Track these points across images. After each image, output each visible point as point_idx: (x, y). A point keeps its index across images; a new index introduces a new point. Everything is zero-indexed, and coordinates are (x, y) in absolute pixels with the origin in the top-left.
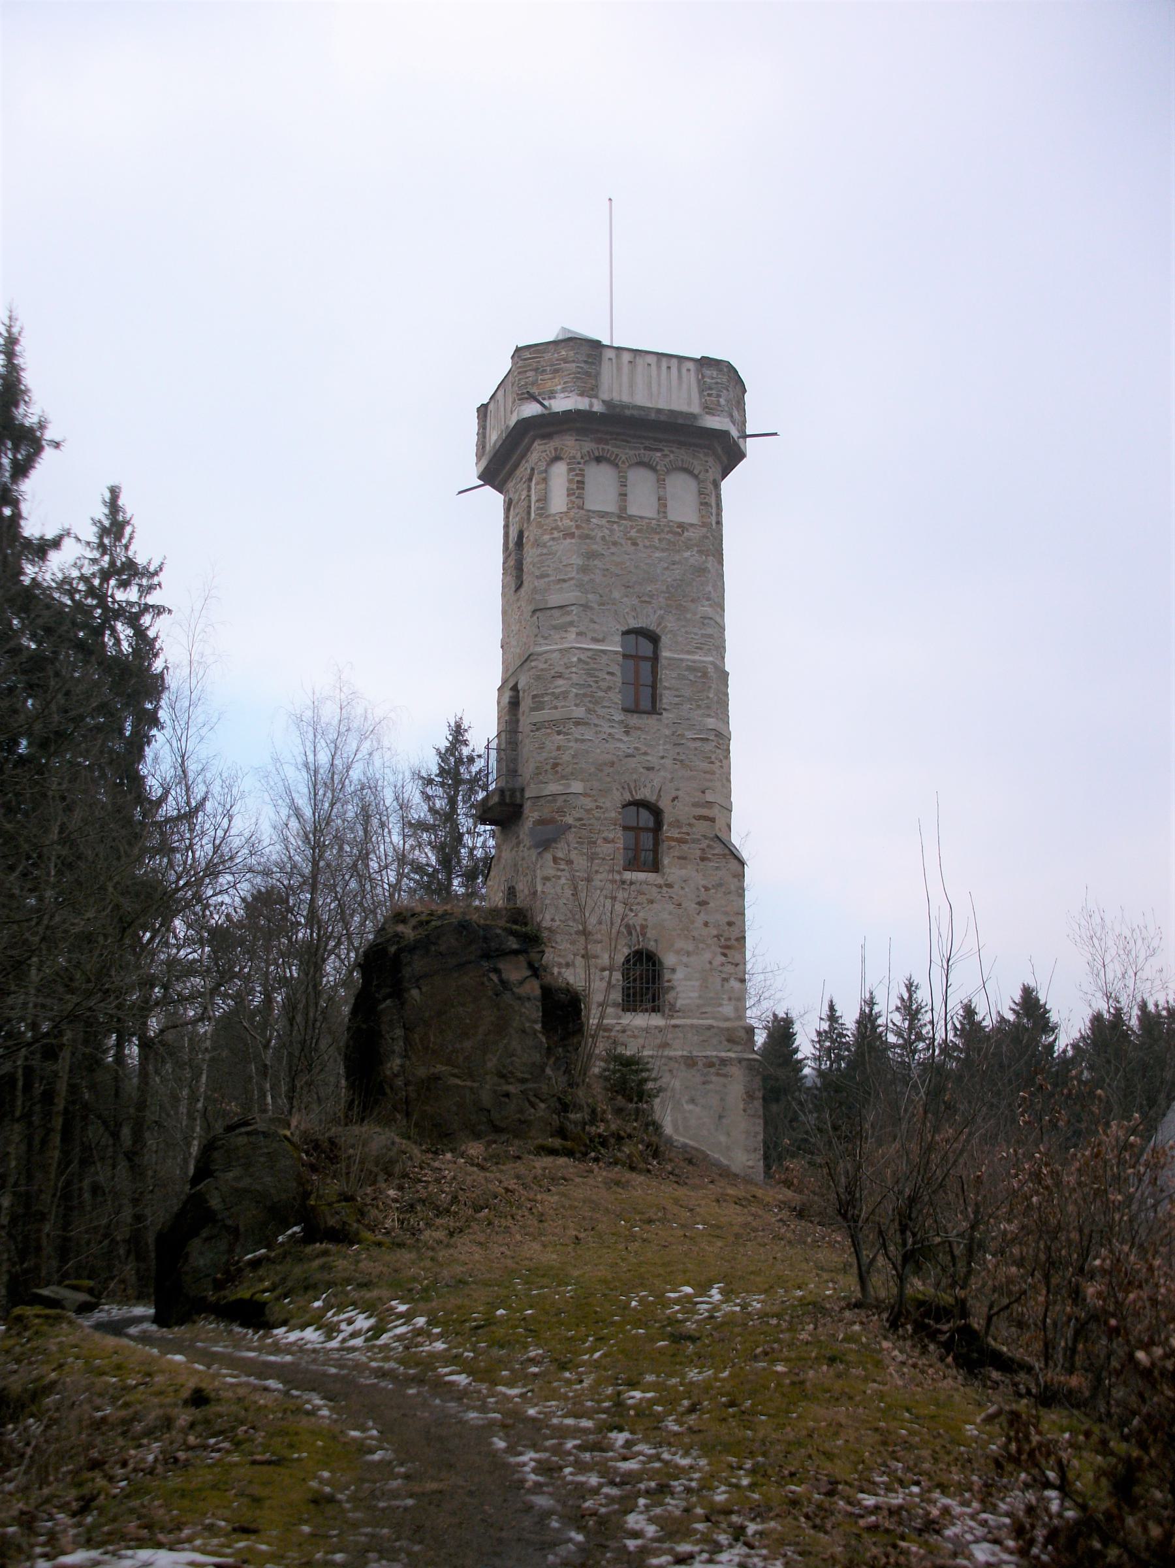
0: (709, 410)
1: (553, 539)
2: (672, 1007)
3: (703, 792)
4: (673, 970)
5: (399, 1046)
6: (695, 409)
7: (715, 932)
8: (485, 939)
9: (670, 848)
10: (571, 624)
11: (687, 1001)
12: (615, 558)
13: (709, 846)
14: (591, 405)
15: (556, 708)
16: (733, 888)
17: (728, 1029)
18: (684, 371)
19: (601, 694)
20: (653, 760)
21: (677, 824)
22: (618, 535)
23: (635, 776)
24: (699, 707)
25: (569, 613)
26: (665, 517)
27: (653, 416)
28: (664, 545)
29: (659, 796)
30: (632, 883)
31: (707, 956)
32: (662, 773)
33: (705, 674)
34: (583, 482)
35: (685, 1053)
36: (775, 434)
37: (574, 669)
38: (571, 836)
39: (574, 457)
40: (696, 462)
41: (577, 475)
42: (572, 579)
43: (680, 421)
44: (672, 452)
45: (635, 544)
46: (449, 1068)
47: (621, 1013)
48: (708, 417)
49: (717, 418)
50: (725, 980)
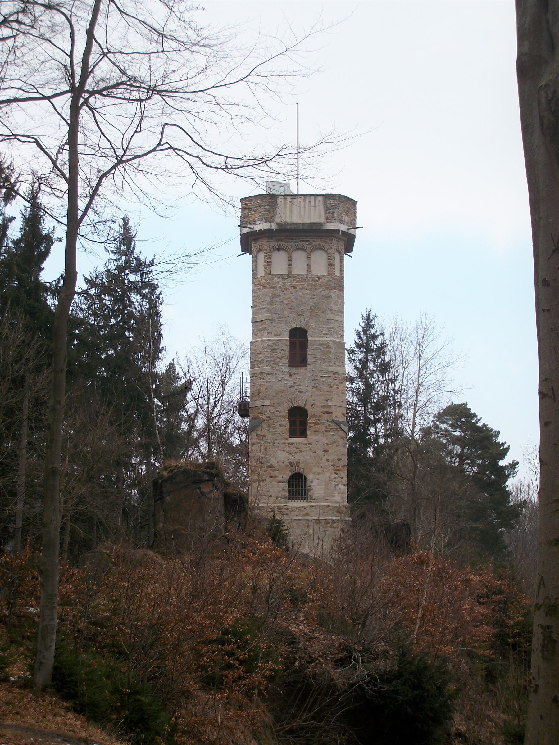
0: (328, 220)
1: (259, 289)
2: (311, 498)
3: (327, 401)
4: (312, 481)
5: (162, 519)
6: (322, 220)
7: (332, 464)
8: (194, 476)
9: (310, 427)
10: (265, 329)
11: (318, 495)
12: (285, 296)
13: (329, 425)
14: (271, 226)
15: (259, 367)
16: (340, 443)
17: (336, 507)
18: (317, 202)
19: (278, 360)
20: (303, 388)
21: (314, 416)
22: (287, 285)
23: (294, 396)
24: (325, 362)
25: (264, 324)
26: (310, 273)
27: (301, 227)
28: (310, 287)
29: (306, 404)
30: (292, 444)
31: (328, 474)
32: (307, 394)
33: (328, 346)
34: (270, 262)
35: (316, 518)
36: (362, 227)
37: (266, 350)
38: (264, 425)
39: (266, 250)
40: (325, 245)
41: (268, 258)
42: (265, 308)
43: (314, 228)
44: (314, 241)
45: (295, 288)
46: (181, 527)
47: (287, 501)
48: (328, 224)
49: (333, 224)
50: (337, 485)
